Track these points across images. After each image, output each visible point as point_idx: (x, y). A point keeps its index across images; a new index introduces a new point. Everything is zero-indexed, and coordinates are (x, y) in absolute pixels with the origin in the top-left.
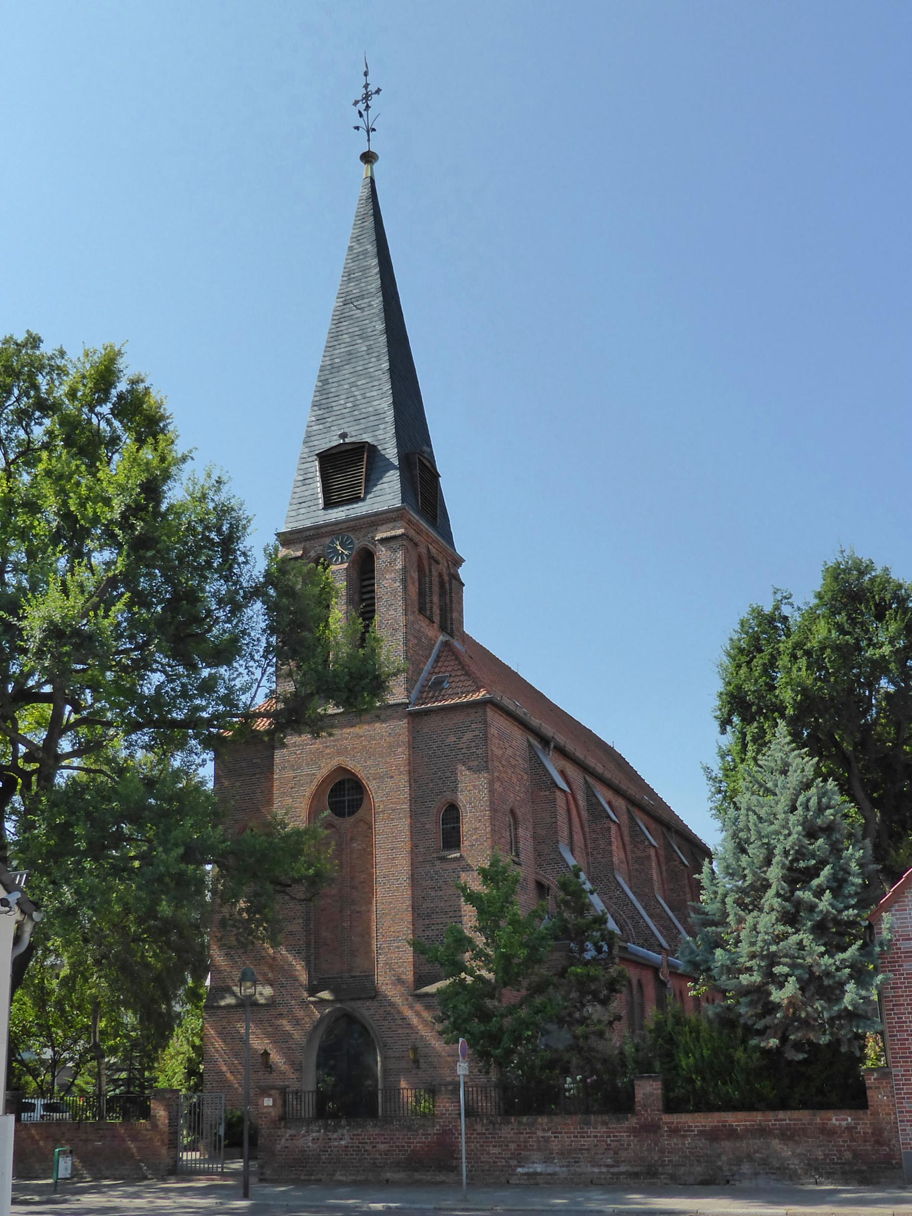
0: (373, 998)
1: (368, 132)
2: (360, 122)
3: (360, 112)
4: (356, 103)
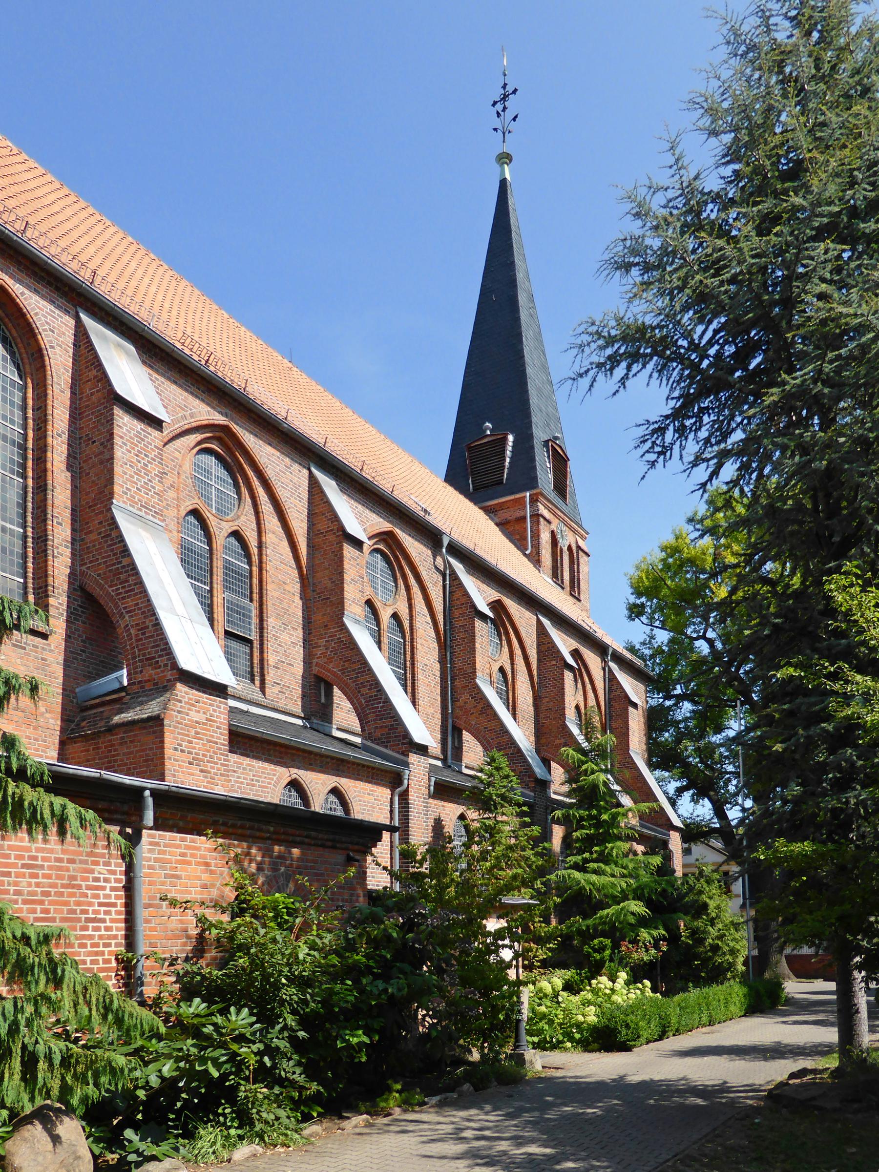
0: (82, 588)
1: (504, 133)
2: (497, 123)
3: (498, 113)
4: (495, 103)
